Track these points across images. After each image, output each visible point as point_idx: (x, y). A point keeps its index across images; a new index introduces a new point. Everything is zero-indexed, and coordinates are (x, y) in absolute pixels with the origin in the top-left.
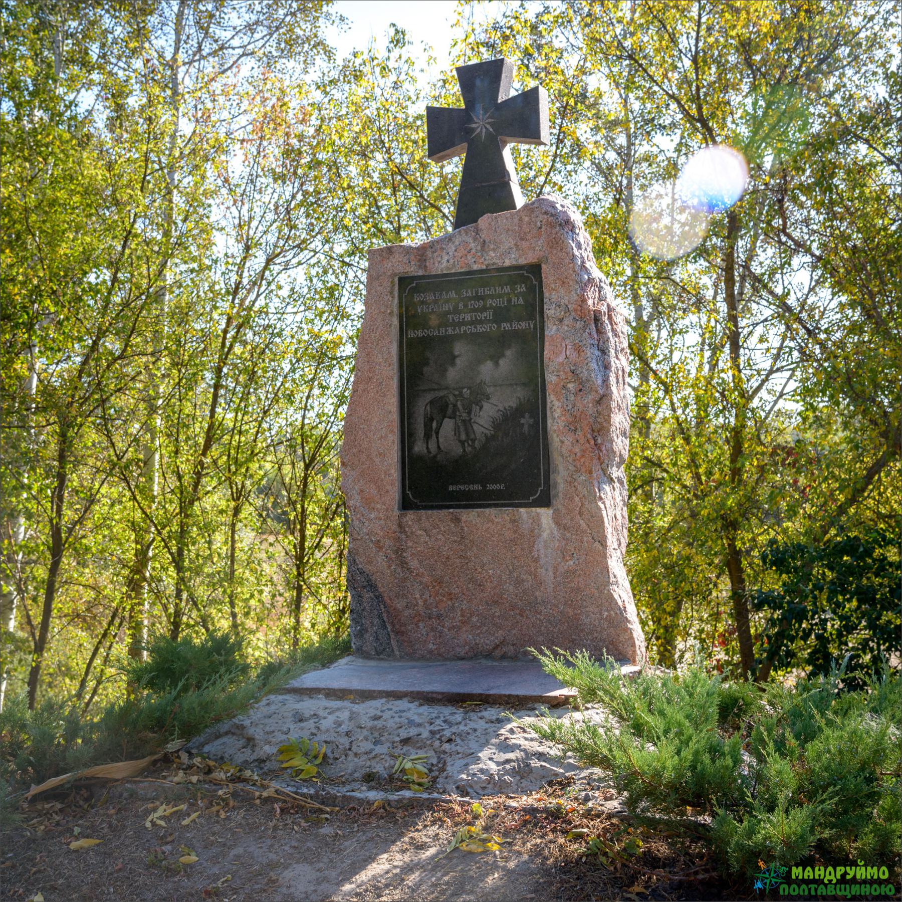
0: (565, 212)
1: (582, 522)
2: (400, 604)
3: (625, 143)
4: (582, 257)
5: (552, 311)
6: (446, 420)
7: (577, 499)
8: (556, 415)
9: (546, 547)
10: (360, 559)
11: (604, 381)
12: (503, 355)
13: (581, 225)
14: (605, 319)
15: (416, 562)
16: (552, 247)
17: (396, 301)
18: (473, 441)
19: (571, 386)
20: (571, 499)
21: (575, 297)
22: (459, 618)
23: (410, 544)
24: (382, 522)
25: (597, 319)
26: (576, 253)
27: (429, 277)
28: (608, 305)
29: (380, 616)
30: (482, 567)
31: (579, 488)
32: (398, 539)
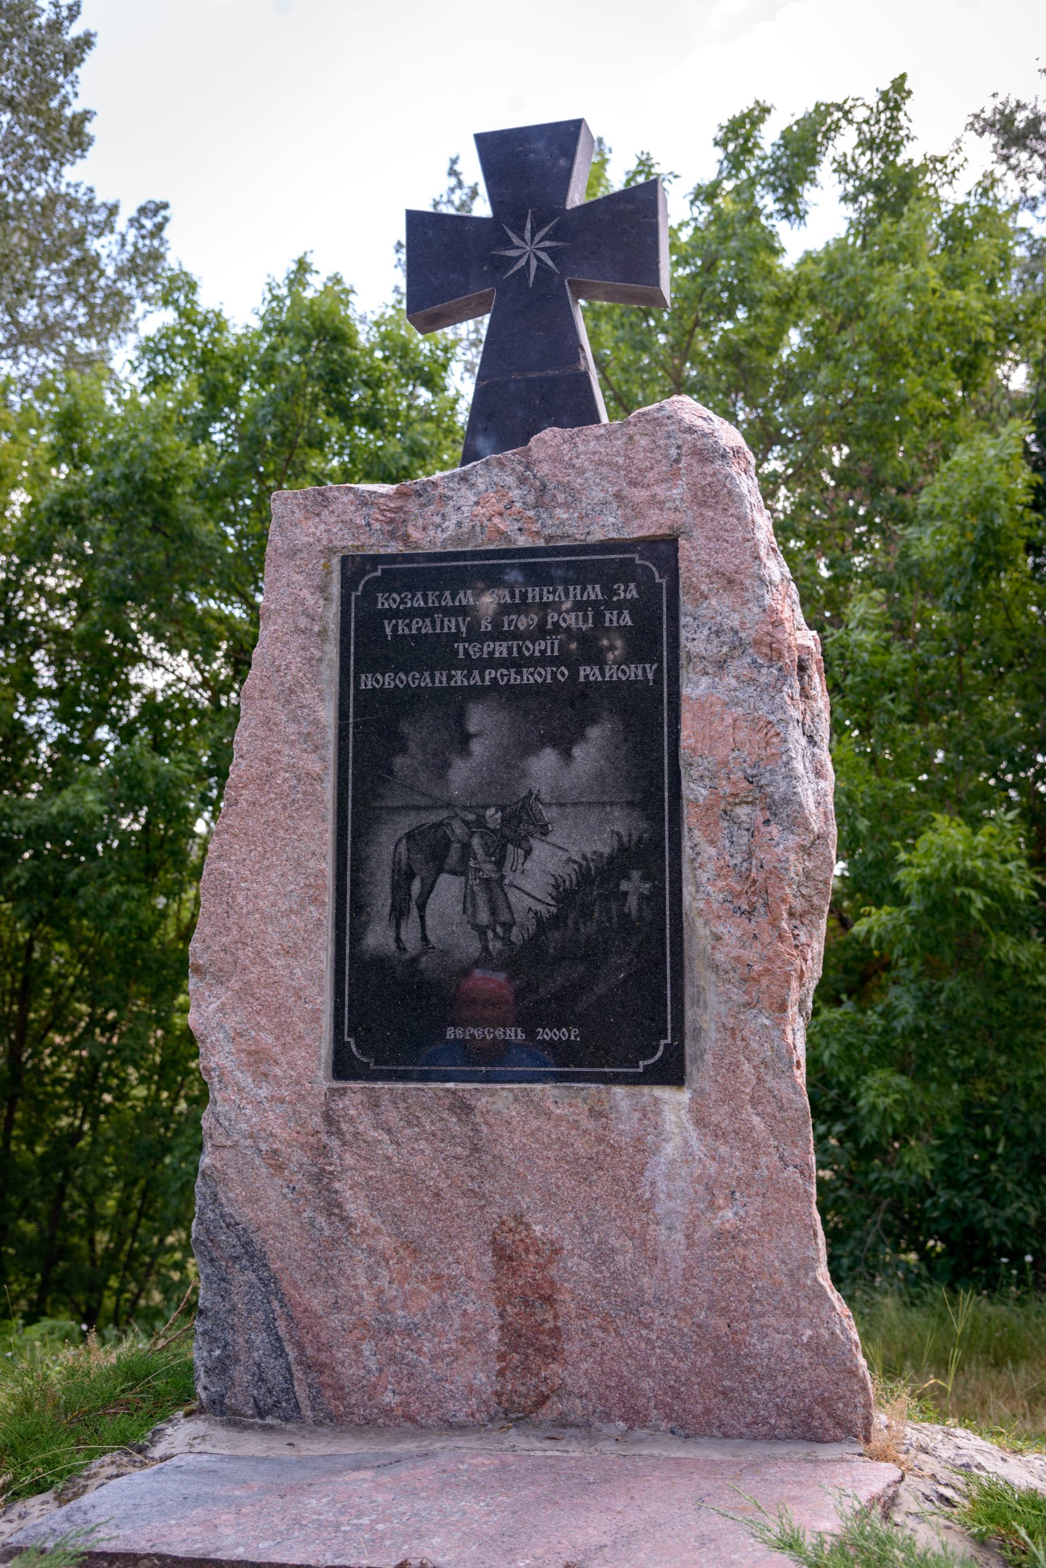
1: (756, 1120)
7: (746, 1067)
12: (579, 736)
17: (335, 607)
18: (507, 927)
20: (734, 1068)
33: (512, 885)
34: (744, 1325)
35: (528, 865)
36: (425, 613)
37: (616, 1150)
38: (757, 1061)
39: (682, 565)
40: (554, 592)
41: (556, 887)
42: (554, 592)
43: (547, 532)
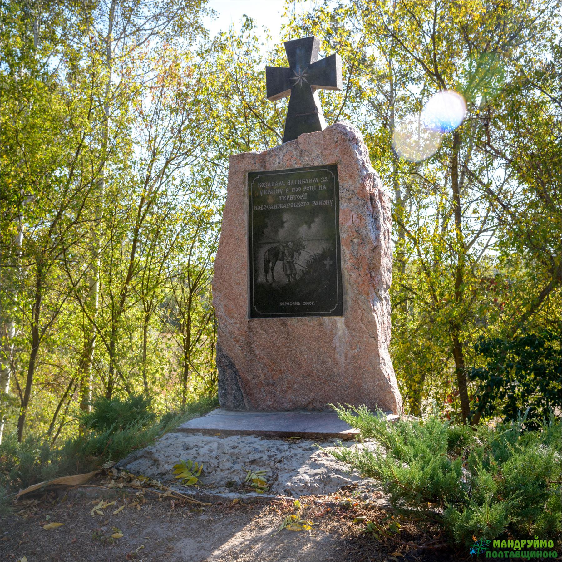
0: (352, 132)
1: (362, 325)
2: (249, 377)
3: (389, 89)
4: (363, 160)
5: (344, 194)
6: (278, 262)
7: (359, 311)
8: (346, 259)
9: (340, 341)
10: (224, 349)
11: (376, 238)
12: (313, 221)
13: (362, 140)
14: (377, 199)
15: (259, 350)
16: (344, 154)
17: (247, 187)
18: (295, 274)
19: (356, 240)
20: (356, 311)
21: (359, 185)
22: (286, 385)
23: (255, 339)
24: (238, 325)
25: (372, 199)
26: (359, 157)
27: (267, 172)
28: (379, 190)
29: (237, 384)
30: (301, 353)
31: (361, 304)
32: (248, 336)
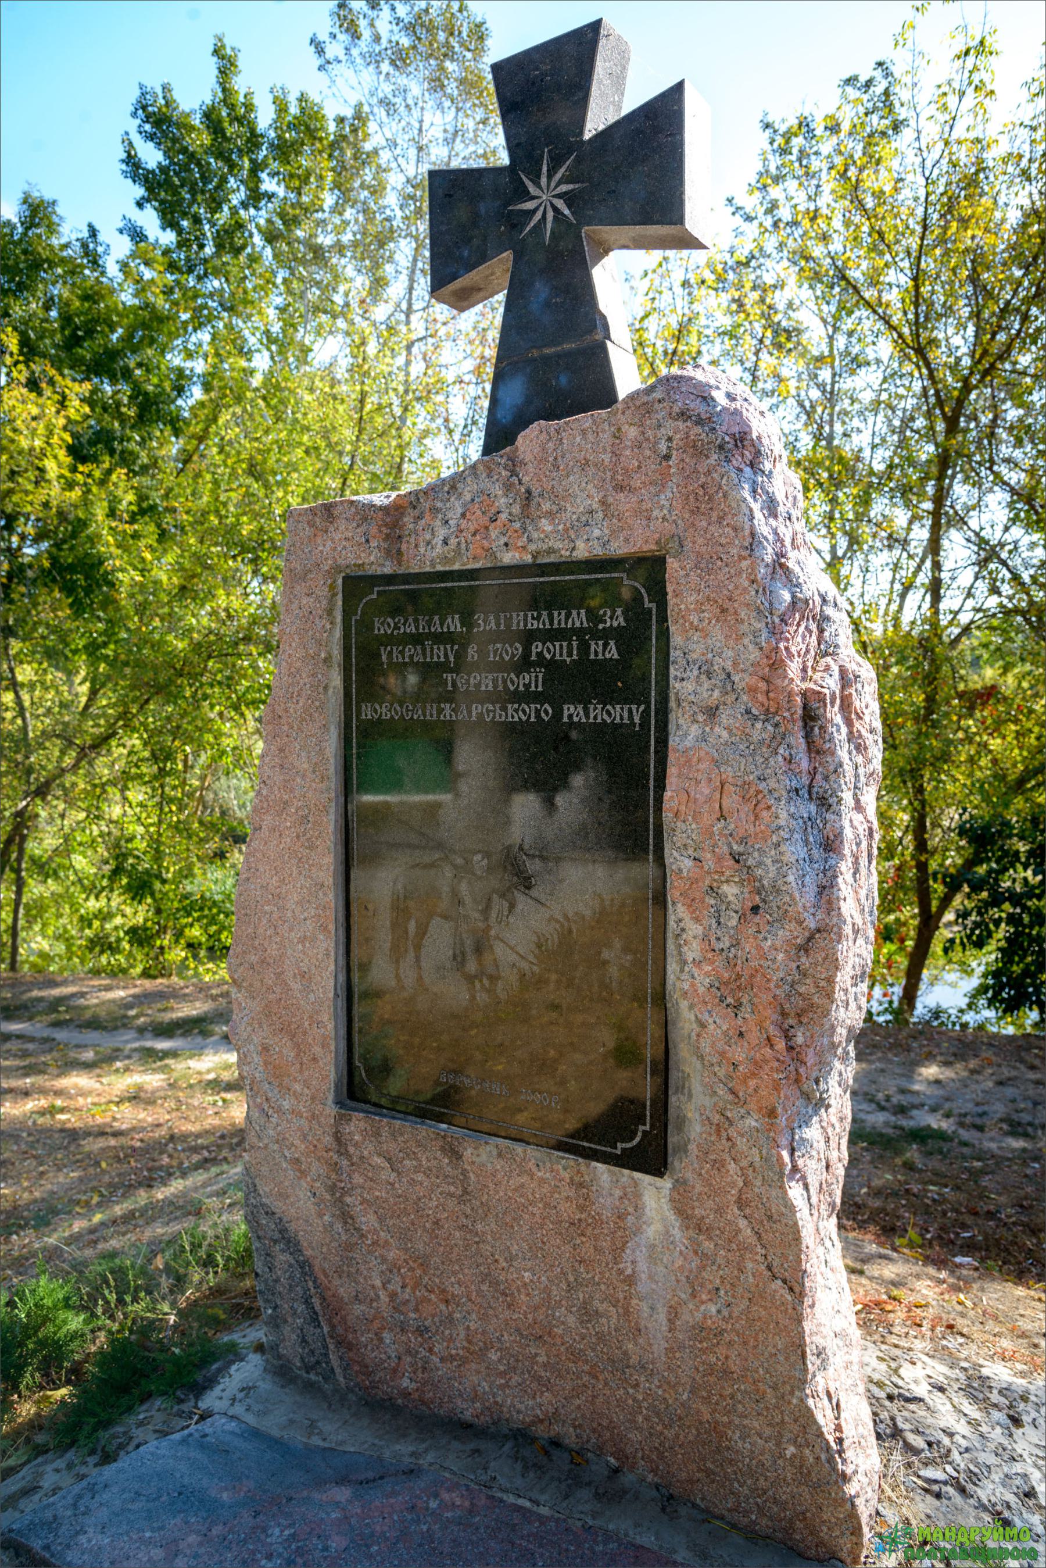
0: (736, 412)
1: (743, 1223)
2: (344, 1290)
3: (829, 381)
4: (779, 540)
5: (689, 686)
6: (436, 921)
7: (732, 1166)
8: (690, 957)
9: (652, 1259)
10: (263, 1188)
11: (822, 889)
12: (563, 783)
13: (779, 448)
14: (834, 714)
15: (372, 1218)
16: (695, 511)
17: (338, 633)
18: (493, 979)
19: (730, 891)
20: (719, 1165)
21: (754, 655)
22: (461, 1340)
23: (357, 1179)
24: (303, 1122)
25: (811, 716)
26: (763, 526)
27: (407, 578)
28: (843, 671)
29: (307, 1302)
30: (510, 1259)
31: (741, 1143)
32: (335, 1167)
33: (497, 937)
34: (725, 1419)
35: (511, 920)
36: (417, 639)
37: (598, 1222)
38: (744, 1163)
39: (670, 589)
40: (538, 619)
41: (539, 946)
42: (538, 619)
43: (532, 547)
